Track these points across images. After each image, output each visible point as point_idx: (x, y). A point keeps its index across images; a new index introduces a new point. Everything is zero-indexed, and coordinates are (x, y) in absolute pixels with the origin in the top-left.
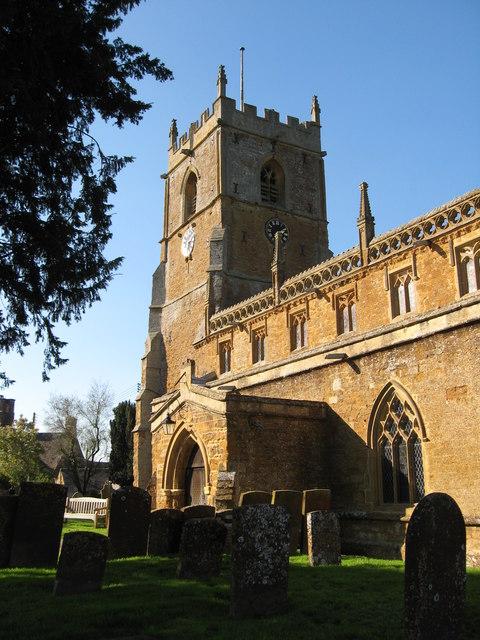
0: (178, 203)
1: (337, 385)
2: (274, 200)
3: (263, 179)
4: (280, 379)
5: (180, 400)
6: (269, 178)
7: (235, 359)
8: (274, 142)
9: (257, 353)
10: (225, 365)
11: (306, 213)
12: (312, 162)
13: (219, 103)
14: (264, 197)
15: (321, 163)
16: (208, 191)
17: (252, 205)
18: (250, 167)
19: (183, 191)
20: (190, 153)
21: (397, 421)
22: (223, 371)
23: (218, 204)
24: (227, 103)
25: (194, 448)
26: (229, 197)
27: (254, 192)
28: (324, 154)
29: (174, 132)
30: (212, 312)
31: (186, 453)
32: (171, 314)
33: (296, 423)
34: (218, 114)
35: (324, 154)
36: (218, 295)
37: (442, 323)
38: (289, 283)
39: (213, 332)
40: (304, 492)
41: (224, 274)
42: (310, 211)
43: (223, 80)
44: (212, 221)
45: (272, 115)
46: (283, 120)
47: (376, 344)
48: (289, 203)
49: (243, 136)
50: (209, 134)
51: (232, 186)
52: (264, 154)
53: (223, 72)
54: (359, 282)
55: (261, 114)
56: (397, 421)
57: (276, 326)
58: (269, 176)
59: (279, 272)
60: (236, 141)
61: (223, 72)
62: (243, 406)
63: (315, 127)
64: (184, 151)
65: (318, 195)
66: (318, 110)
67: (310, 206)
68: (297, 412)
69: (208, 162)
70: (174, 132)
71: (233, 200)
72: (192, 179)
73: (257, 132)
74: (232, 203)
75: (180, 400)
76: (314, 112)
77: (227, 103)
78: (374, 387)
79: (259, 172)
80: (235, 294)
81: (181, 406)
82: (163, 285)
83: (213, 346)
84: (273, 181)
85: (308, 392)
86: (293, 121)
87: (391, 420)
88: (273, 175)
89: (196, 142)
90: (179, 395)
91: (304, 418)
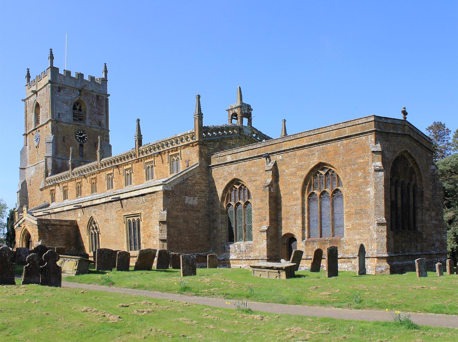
0: (32, 116)
1: (79, 215)
2: (80, 120)
3: (74, 108)
4: (64, 211)
5: (23, 219)
6: (77, 108)
7: (57, 198)
8: (80, 91)
9: (65, 197)
10: (53, 200)
11: (98, 126)
12: (101, 100)
13: (50, 70)
14: (75, 118)
15: (107, 100)
16: (45, 114)
17: (67, 124)
18: (67, 104)
19: (34, 112)
20: (35, 92)
21: (94, 227)
22: (52, 202)
23: (50, 123)
24: (54, 71)
25: (30, 236)
26: (56, 121)
27: (69, 117)
28: (109, 95)
29: (28, 76)
30: (47, 176)
31: (27, 238)
32: (31, 172)
33: (65, 227)
34: (49, 78)
35: (109, 95)
36: (50, 168)
37: (103, 200)
38: (76, 170)
39: (47, 185)
40: (416, 261)
41: (54, 157)
42: (100, 125)
43: (52, 57)
44: (47, 133)
45: (81, 76)
46: (86, 78)
47: (89, 203)
48: (88, 122)
49: (62, 88)
50: (45, 86)
51: (57, 114)
52: (75, 96)
53: (51, 52)
54: (98, 175)
55: (73, 75)
56: (94, 227)
57: (71, 186)
58: (78, 107)
59: (72, 164)
60: (59, 91)
61: (51, 52)
62: (43, 222)
63: (105, 80)
64: (33, 91)
65: (104, 117)
66: (106, 72)
67: (100, 123)
68: (65, 223)
69: (45, 100)
70: (28, 76)
71: (57, 122)
72: (37, 106)
73: (70, 85)
74: (57, 122)
75: (23, 219)
76: (104, 73)
77: (54, 71)
78: (89, 217)
79: (72, 107)
80: (59, 166)
81: (24, 221)
82: (26, 157)
83: (47, 191)
84: (80, 110)
85: (70, 217)
86: (92, 78)
87: (93, 227)
88: (80, 107)
89: (39, 87)
90: (23, 217)
91: (68, 226)
